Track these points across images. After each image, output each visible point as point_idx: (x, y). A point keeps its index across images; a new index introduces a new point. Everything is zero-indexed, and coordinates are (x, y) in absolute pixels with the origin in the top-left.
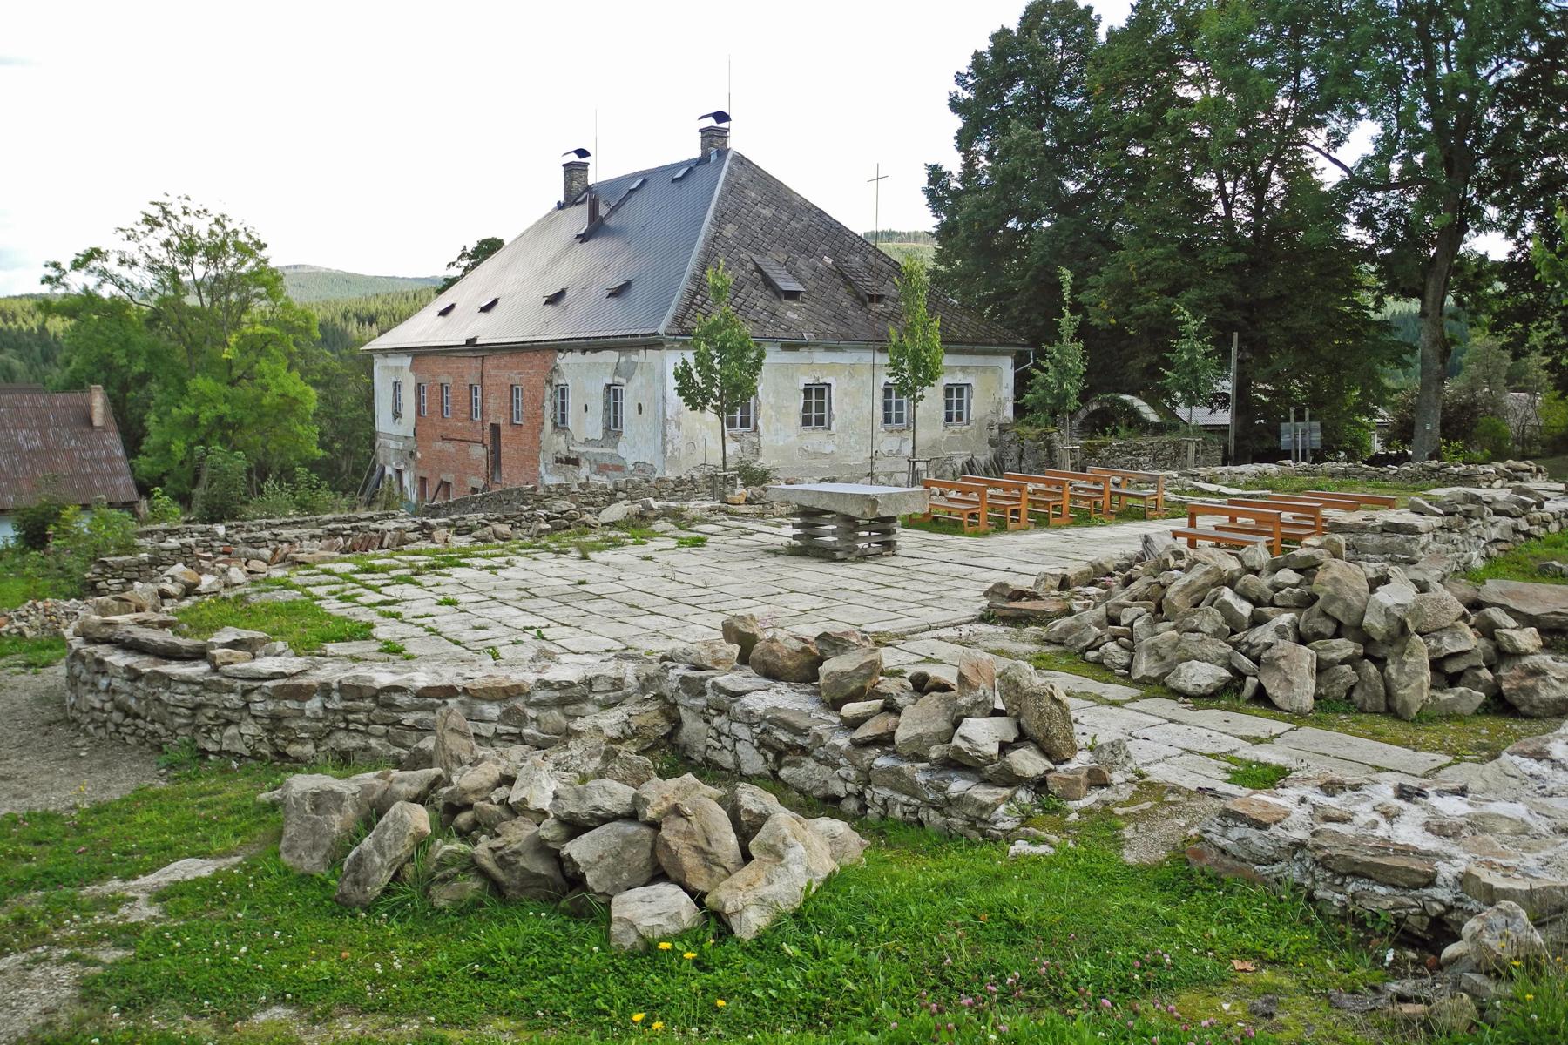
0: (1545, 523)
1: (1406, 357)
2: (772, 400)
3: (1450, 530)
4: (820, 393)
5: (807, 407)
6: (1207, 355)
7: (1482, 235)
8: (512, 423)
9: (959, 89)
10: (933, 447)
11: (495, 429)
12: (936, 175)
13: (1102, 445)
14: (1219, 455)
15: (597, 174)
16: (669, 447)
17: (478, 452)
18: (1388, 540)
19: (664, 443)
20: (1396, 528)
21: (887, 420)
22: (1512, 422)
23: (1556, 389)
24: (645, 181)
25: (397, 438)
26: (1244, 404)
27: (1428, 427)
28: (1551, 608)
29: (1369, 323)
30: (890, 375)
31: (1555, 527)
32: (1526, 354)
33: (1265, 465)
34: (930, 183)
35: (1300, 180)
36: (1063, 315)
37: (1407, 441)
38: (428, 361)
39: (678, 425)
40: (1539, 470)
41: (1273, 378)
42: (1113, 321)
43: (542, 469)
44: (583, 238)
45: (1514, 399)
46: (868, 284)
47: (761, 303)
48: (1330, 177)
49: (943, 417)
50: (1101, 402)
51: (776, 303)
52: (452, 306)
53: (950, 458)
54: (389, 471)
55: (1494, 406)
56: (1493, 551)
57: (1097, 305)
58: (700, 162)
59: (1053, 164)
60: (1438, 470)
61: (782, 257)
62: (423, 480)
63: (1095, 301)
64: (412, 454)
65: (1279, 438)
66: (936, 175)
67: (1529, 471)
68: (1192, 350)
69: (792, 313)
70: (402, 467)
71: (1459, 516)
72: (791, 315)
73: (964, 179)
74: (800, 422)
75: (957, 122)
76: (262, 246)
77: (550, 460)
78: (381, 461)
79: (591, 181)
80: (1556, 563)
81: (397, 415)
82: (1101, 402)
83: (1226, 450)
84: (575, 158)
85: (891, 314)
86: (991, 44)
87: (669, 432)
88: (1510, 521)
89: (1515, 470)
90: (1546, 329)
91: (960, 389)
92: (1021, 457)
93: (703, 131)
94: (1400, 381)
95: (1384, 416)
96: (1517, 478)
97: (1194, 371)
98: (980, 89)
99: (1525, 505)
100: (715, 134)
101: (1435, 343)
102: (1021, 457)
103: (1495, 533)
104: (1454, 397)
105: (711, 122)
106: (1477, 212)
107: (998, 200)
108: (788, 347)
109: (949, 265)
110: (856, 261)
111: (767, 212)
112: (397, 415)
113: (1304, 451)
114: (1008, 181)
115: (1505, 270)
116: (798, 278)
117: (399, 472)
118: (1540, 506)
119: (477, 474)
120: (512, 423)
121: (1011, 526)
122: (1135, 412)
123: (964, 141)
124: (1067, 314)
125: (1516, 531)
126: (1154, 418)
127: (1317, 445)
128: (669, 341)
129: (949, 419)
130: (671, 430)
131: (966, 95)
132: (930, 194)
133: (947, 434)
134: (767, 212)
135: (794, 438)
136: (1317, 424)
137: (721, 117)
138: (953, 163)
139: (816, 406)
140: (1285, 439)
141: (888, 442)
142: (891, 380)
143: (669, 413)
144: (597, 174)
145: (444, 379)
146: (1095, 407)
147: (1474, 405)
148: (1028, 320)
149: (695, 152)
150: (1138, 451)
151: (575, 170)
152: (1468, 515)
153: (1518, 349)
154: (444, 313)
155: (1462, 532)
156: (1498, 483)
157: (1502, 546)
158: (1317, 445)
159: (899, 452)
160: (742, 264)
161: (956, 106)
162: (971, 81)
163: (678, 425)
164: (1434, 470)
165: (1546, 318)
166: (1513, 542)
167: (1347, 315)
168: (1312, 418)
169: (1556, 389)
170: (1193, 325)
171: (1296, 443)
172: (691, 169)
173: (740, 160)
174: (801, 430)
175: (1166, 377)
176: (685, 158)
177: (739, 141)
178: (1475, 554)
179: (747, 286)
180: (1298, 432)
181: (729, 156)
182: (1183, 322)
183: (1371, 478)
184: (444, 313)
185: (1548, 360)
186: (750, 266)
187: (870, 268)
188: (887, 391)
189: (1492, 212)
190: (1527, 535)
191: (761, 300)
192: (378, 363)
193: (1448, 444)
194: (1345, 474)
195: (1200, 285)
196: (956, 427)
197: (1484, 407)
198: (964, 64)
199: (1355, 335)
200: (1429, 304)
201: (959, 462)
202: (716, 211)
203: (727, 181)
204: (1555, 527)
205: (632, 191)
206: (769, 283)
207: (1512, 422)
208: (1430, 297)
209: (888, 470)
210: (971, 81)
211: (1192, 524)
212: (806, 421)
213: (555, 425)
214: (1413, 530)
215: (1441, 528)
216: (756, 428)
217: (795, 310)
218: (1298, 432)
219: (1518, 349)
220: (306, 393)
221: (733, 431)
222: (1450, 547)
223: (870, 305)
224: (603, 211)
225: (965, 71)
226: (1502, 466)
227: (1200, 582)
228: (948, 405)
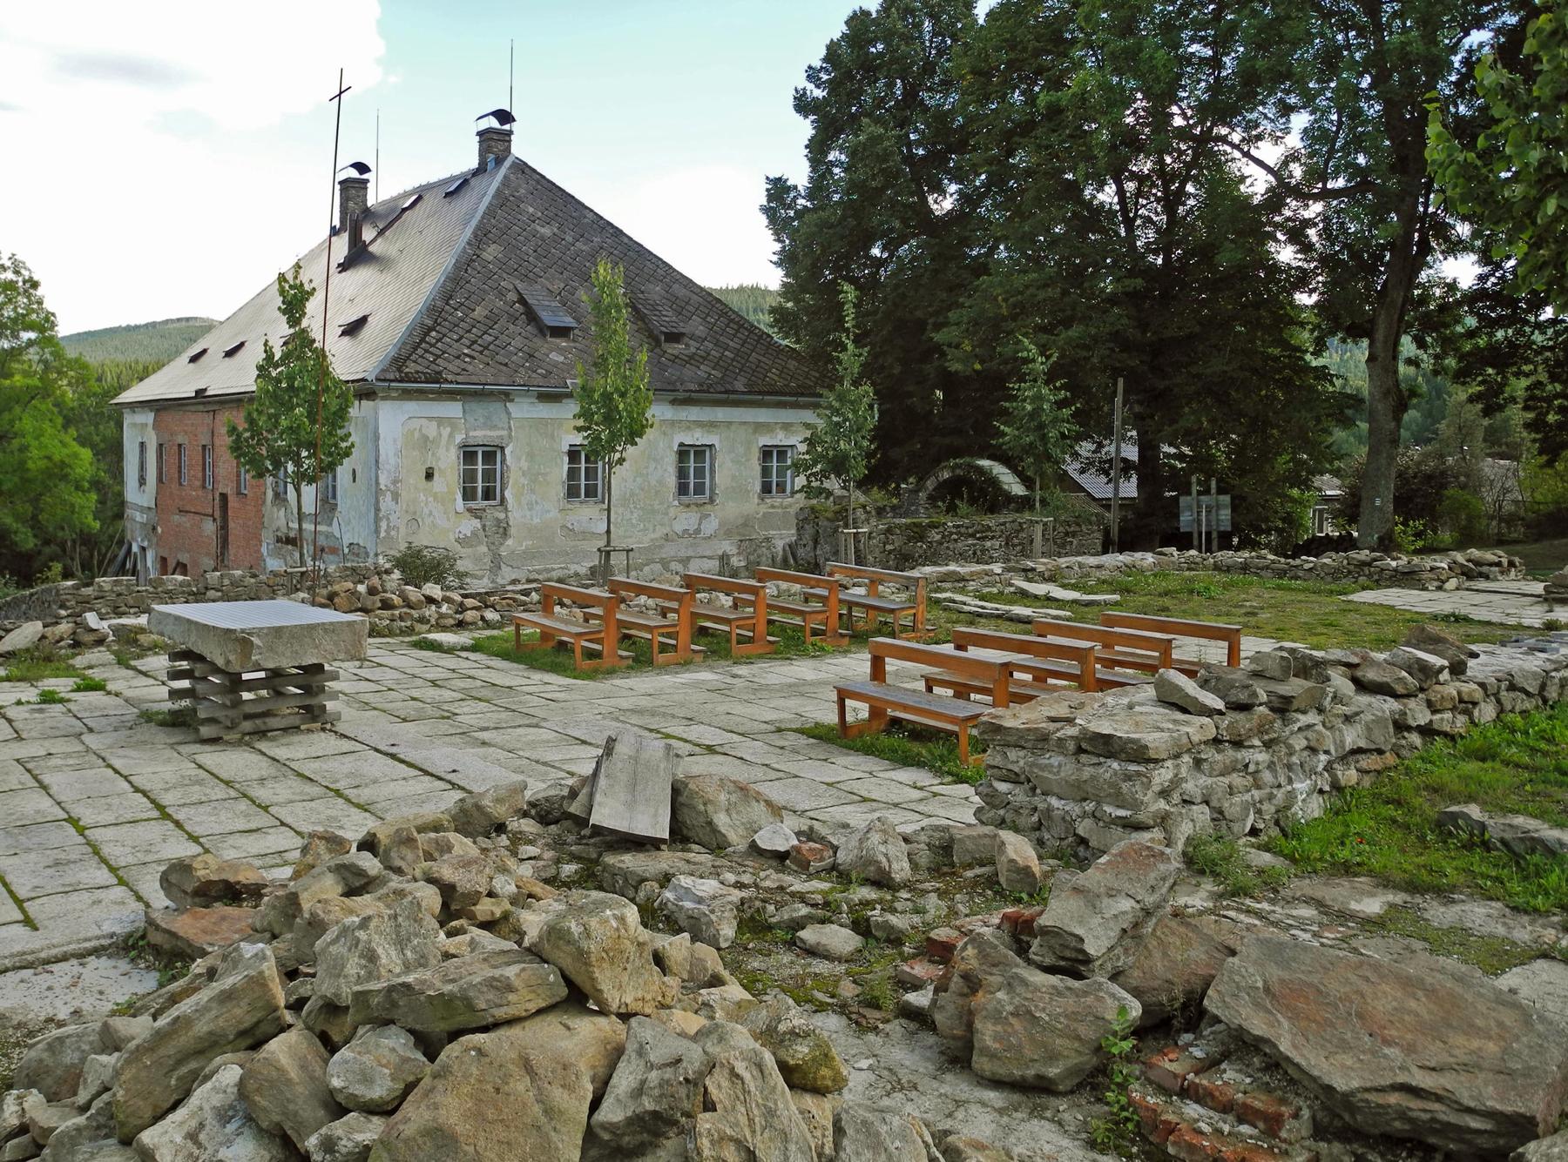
0: (1465, 705)
1: (1349, 412)
2: (524, 464)
3: (1238, 744)
4: (489, 457)
5: (573, 474)
6: (1061, 404)
7: (1451, 259)
8: (239, 493)
9: (810, 86)
10: (745, 525)
11: (224, 497)
12: (779, 190)
13: (933, 526)
14: (1097, 538)
15: (379, 193)
16: (384, 525)
17: (210, 527)
18: (1088, 772)
19: (377, 520)
20: (1105, 746)
21: (682, 489)
22: (1489, 497)
23: (1540, 453)
24: (419, 198)
25: (142, 509)
26: (1148, 468)
27: (1378, 503)
28: (1397, 1065)
29: (1307, 368)
30: (579, 429)
31: (1487, 712)
32: (1501, 408)
33: (1139, 555)
34: (770, 198)
35: (1222, 187)
36: (845, 349)
37: (1353, 519)
38: (169, 417)
39: (396, 497)
40: (1511, 564)
41: (1190, 436)
42: (978, 367)
43: (264, 550)
44: (344, 267)
45: (1492, 468)
46: (667, 319)
47: (518, 342)
48: (1258, 184)
49: (758, 488)
50: (953, 469)
51: (538, 341)
52: (204, 351)
53: (768, 539)
54: (135, 548)
55: (1467, 476)
56: (1348, 776)
57: (957, 346)
58: (476, 173)
59: (928, 175)
60: (1369, 564)
61: (558, 285)
62: (164, 560)
63: (956, 340)
64: (154, 529)
65: (1177, 516)
66: (779, 190)
67: (1499, 564)
68: (1039, 398)
69: (556, 353)
70: (145, 544)
71: (1256, 709)
72: (556, 357)
73: (811, 195)
74: (561, 491)
75: (805, 128)
76: (35, 285)
77: (271, 540)
78: (129, 537)
79: (371, 201)
80: (1474, 811)
81: (142, 481)
82: (953, 469)
83: (1107, 532)
84: (354, 174)
85: (691, 357)
86: (844, 28)
87: (383, 506)
88: (1390, 705)
89: (1478, 563)
90: (1527, 375)
91: (700, 451)
92: (816, 542)
93: (480, 134)
94: (1351, 441)
95: (1331, 487)
96: (1482, 575)
97: (1041, 426)
98: (833, 86)
99: (1426, 672)
100: (495, 140)
101: (1387, 394)
102: (816, 542)
103: (1352, 737)
104: (1419, 464)
105: (493, 123)
106: (1442, 230)
107: (844, 218)
108: (545, 397)
109: (797, 301)
110: (655, 291)
111: (546, 231)
112: (142, 481)
113: (1209, 534)
114: (863, 196)
115: (1474, 297)
116: (573, 311)
117: (143, 549)
118: (1458, 669)
119: (208, 554)
120: (239, 493)
121: (661, 658)
122: (994, 482)
123: (817, 150)
124: (850, 346)
125: (1401, 726)
126: (1018, 489)
127: (1226, 526)
128: (383, 389)
129: (766, 489)
130: (386, 503)
131: (819, 93)
132: (768, 211)
133: (763, 509)
134: (546, 231)
135: (554, 514)
136: (1226, 499)
137: (504, 116)
138: (799, 174)
139: (692, 471)
140: (1185, 518)
141: (686, 520)
142: (578, 439)
143: (383, 480)
144: (379, 193)
145: (180, 439)
146: (946, 475)
147: (1443, 473)
148: (882, 367)
149: (473, 162)
150: (984, 534)
151: (352, 189)
152: (1283, 707)
153: (1491, 402)
154: (194, 359)
155: (1267, 745)
156: (1452, 583)
157: (1367, 762)
158: (1226, 526)
159: (698, 531)
160: (501, 294)
161: (803, 105)
162: (825, 77)
163: (396, 497)
164: (1363, 564)
165: (1527, 361)
166: (1396, 751)
167: (1276, 359)
168: (1220, 491)
169: (1540, 453)
170: (1040, 365)
171: (1200, 525)
172: (465, 182)
173: (522, 168)
174: (563, 503)
175: (1004, 434)
176: (456, 172)
177: (521, 148)
178: (1302, 786)
179: (503, 321)
180: (1203, 509)
181: (507, 163)
182: (1026, 361)
183: (1282, 574)
184: (194, 359)
185: (1531, 415)
186: (512, 296)
187: (673, 300)
188: (573, 455)
189: (1463, 230)
190: (1427, 731)
191: (518, 337)
192: (129, 419)
193: (1405, 524)
194: (1245, 568)
195: (1085, 319)
196: (776, 500)
197: (1457, 478)
198: (816, 57)
199: (1286, 384)
200: (1378, 345)
201: (780, 544)
202: (478, 228)
203: (499, 192)
204: (1487, 712)
205: (404, 210)
206: (532, 316)
207: (1489, 497)
208: (1380, 335)
209: (683, 554)
210: (825, 77)
211: (878, 672)
212: (572, 492)
213: (277, 495)
214: (1138, 754)
215: (1216, 741)
216: (503, 499)
217: (561, 351)
218: (1203, 509)
219: (1491, 402)
220: (76, 455)
221: (472, 504)
222: (1237, 780)
223: (665, 346)
224: (368, 234)
225: (817, 64)
226: (1460, 557)
227: (202, 1027)
228: (766, 472)
